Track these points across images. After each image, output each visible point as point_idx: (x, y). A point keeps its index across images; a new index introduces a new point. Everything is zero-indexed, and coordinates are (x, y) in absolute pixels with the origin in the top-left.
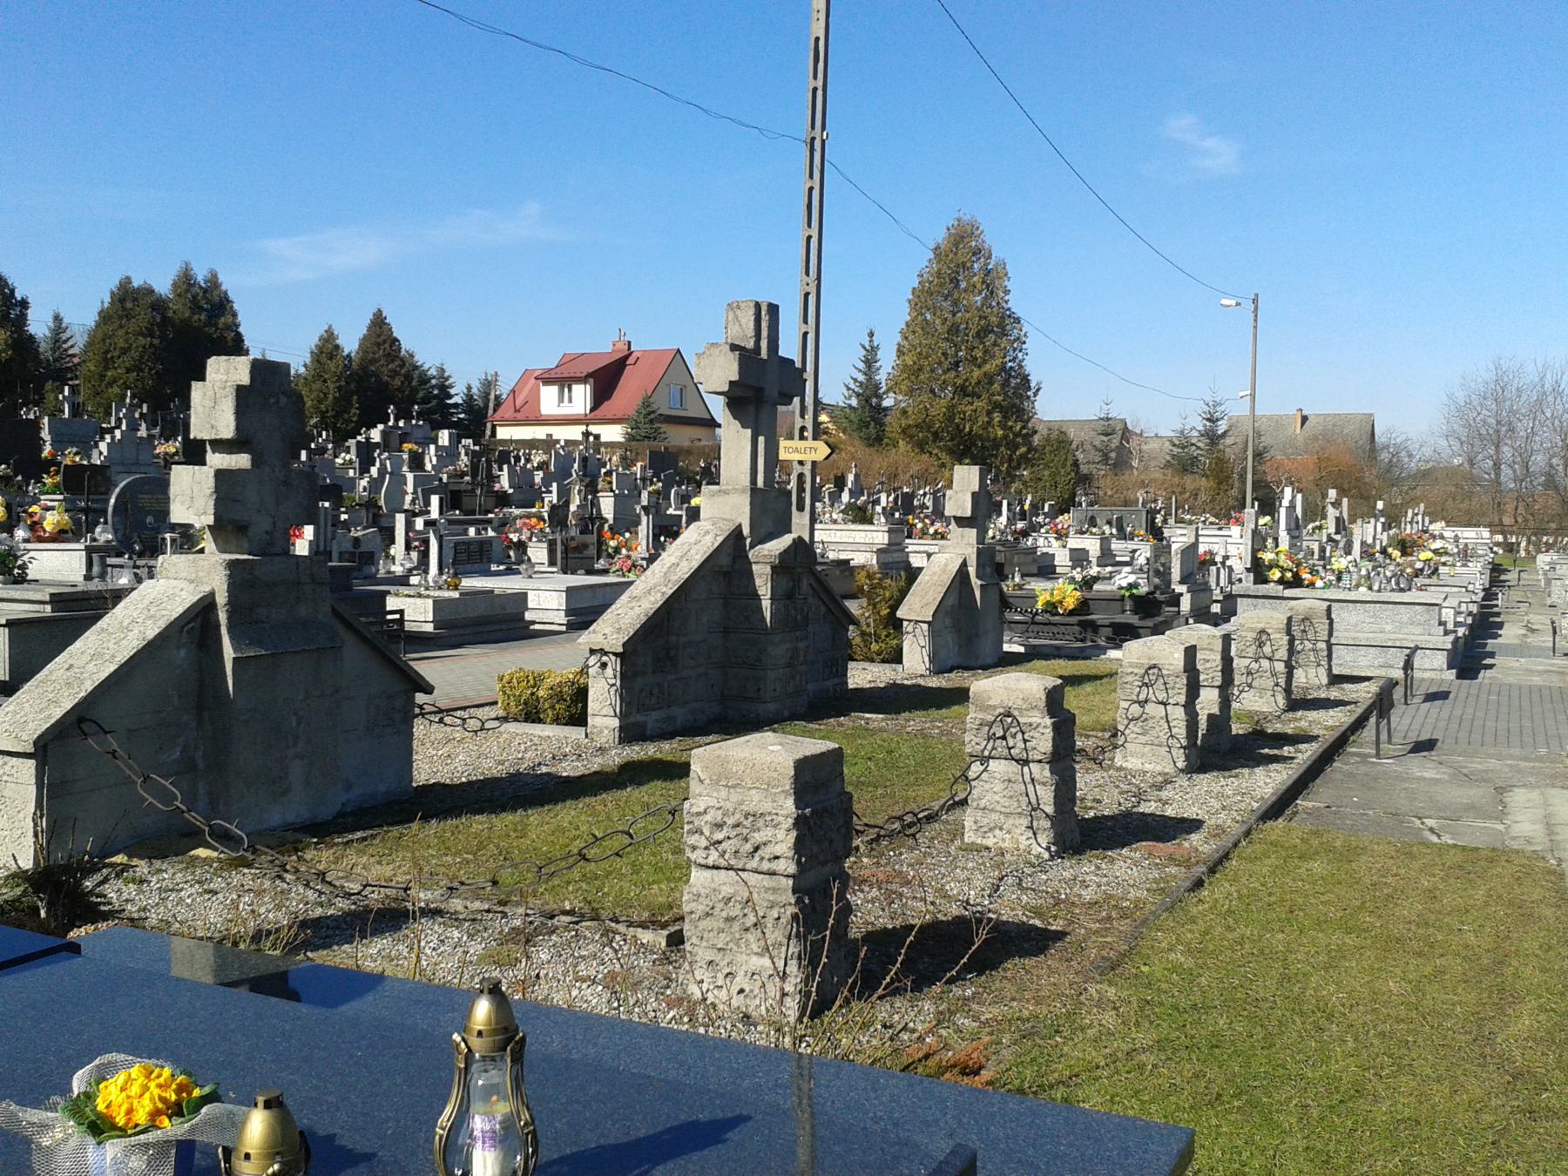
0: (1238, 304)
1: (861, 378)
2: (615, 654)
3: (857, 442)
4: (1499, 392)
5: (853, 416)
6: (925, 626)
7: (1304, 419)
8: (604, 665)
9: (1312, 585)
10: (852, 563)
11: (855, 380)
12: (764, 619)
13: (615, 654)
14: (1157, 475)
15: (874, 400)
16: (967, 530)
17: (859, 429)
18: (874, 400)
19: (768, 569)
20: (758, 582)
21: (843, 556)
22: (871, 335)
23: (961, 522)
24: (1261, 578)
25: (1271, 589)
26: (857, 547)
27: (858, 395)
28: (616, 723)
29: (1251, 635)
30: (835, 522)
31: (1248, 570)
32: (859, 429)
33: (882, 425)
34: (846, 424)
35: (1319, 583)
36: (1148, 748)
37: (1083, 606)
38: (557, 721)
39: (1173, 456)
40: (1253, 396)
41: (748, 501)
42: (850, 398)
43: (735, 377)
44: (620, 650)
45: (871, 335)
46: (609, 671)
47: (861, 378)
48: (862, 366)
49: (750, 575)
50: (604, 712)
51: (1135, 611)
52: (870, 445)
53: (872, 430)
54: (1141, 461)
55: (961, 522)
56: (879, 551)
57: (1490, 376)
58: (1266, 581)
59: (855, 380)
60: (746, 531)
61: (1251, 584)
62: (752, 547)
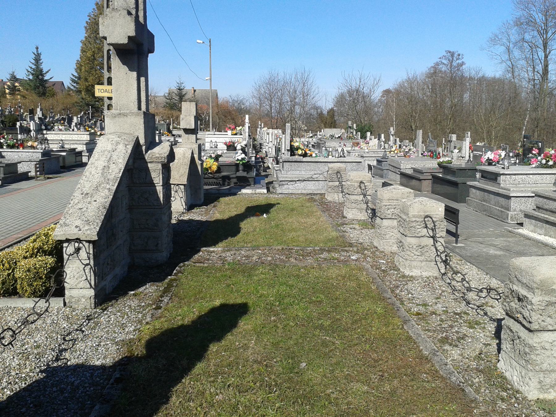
0: (203, 43)
1: (34, 67)
2: (89, 242)
3: (34, 95)
4: (271, 82)
5: (31, 84)
6: (182, 187)
7: (195, 91)
8: (78, 250)
9: (311, 155)
10: (77, 150)
11: (31, 68)
12: (158, 198)
13: (89, 242)
14: (161, 110)
15: (40, 77)
16: (191, 136)
17: (35, 89)
18: (40, 77)
19: (160, 166)
20: (153, 175)
21: (73, 147)
22: (37, 48)
23: (187, 131)
24: (293, 154)
25: (296, 158)
26: (78, 142)
27: (33, 74)
28: (92, 292)
29: (357, 185)
30: (61, 130)
31: (288, 150)
32: (35, 89)
33: (45, 87)
34: (28, 87)
35: (314, 155)
36: (424, 263)
37: (219, 170)
38: (34, 294)
39: (167, 103)
40: (211, 79)
41: (142, 121)
42: (29, 75)
43: (132, 33)
44: (96, 238)
45: (37, 48)
46: (83, 254)
47: (34, 67)
48: (33, 61)
49: (147, 170)
50: (81, 285)
51: (244, 171)
52: (40, 96)
53: (41, 90)
54: (155, 104)
55: (187, 131)
56: (86, 144)
57: (267, 77)
58: (294, 155)
59: (31, 68)
60: (142, 141)
61: (289, 156)
62: (146, 152)
